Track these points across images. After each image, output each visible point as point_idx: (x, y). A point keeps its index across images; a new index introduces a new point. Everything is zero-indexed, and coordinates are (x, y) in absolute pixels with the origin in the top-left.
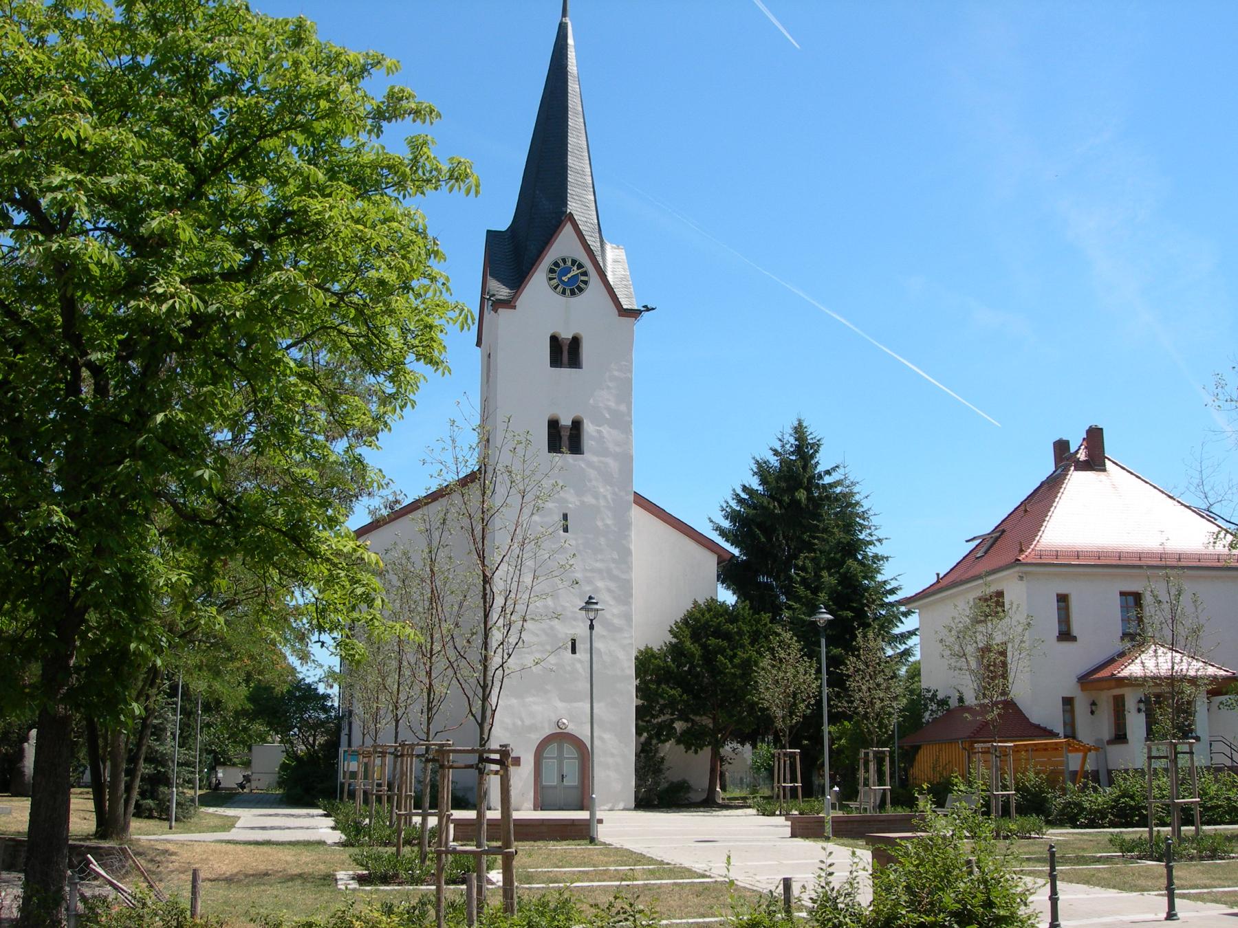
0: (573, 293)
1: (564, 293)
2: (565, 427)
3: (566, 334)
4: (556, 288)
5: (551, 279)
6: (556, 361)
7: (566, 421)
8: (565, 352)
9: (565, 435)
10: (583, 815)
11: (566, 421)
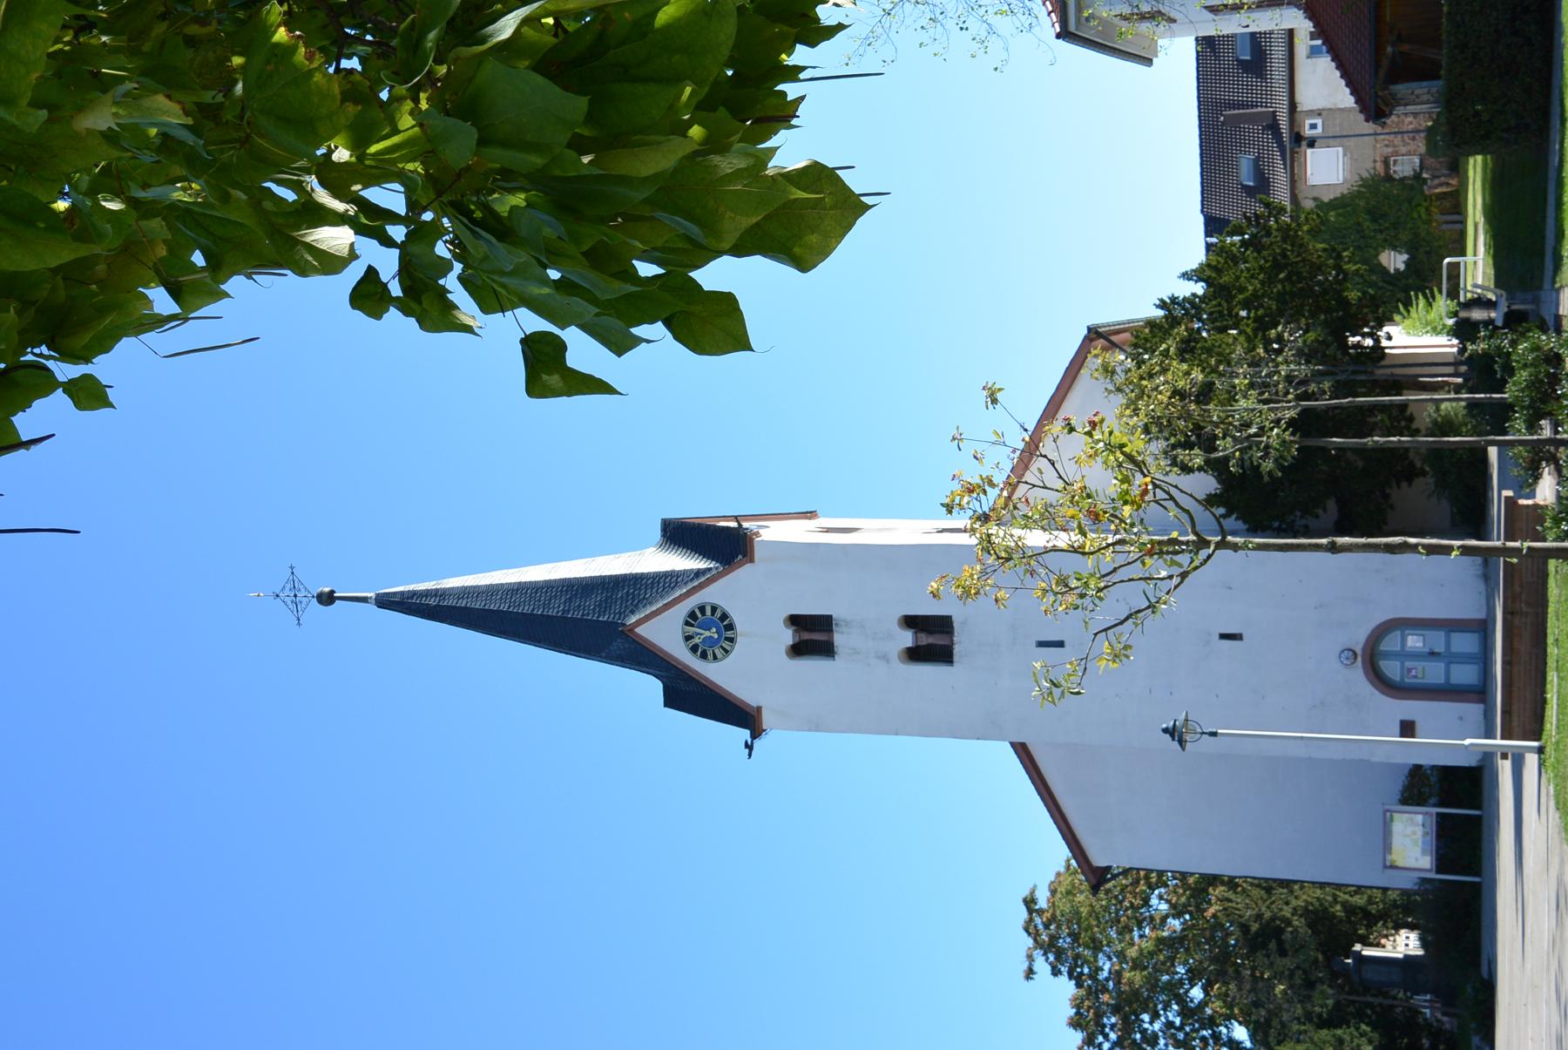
0: (730, 627)
1: (731, 640)
2: (916, 639)
3: (788, 637)
4: (727, 651)
5: (715, 658)
6: (826, 650)
7: (907, 638)
8: (812, 636)
9: (925, 640)
10: (1476, 879)
11: (907, 638)
